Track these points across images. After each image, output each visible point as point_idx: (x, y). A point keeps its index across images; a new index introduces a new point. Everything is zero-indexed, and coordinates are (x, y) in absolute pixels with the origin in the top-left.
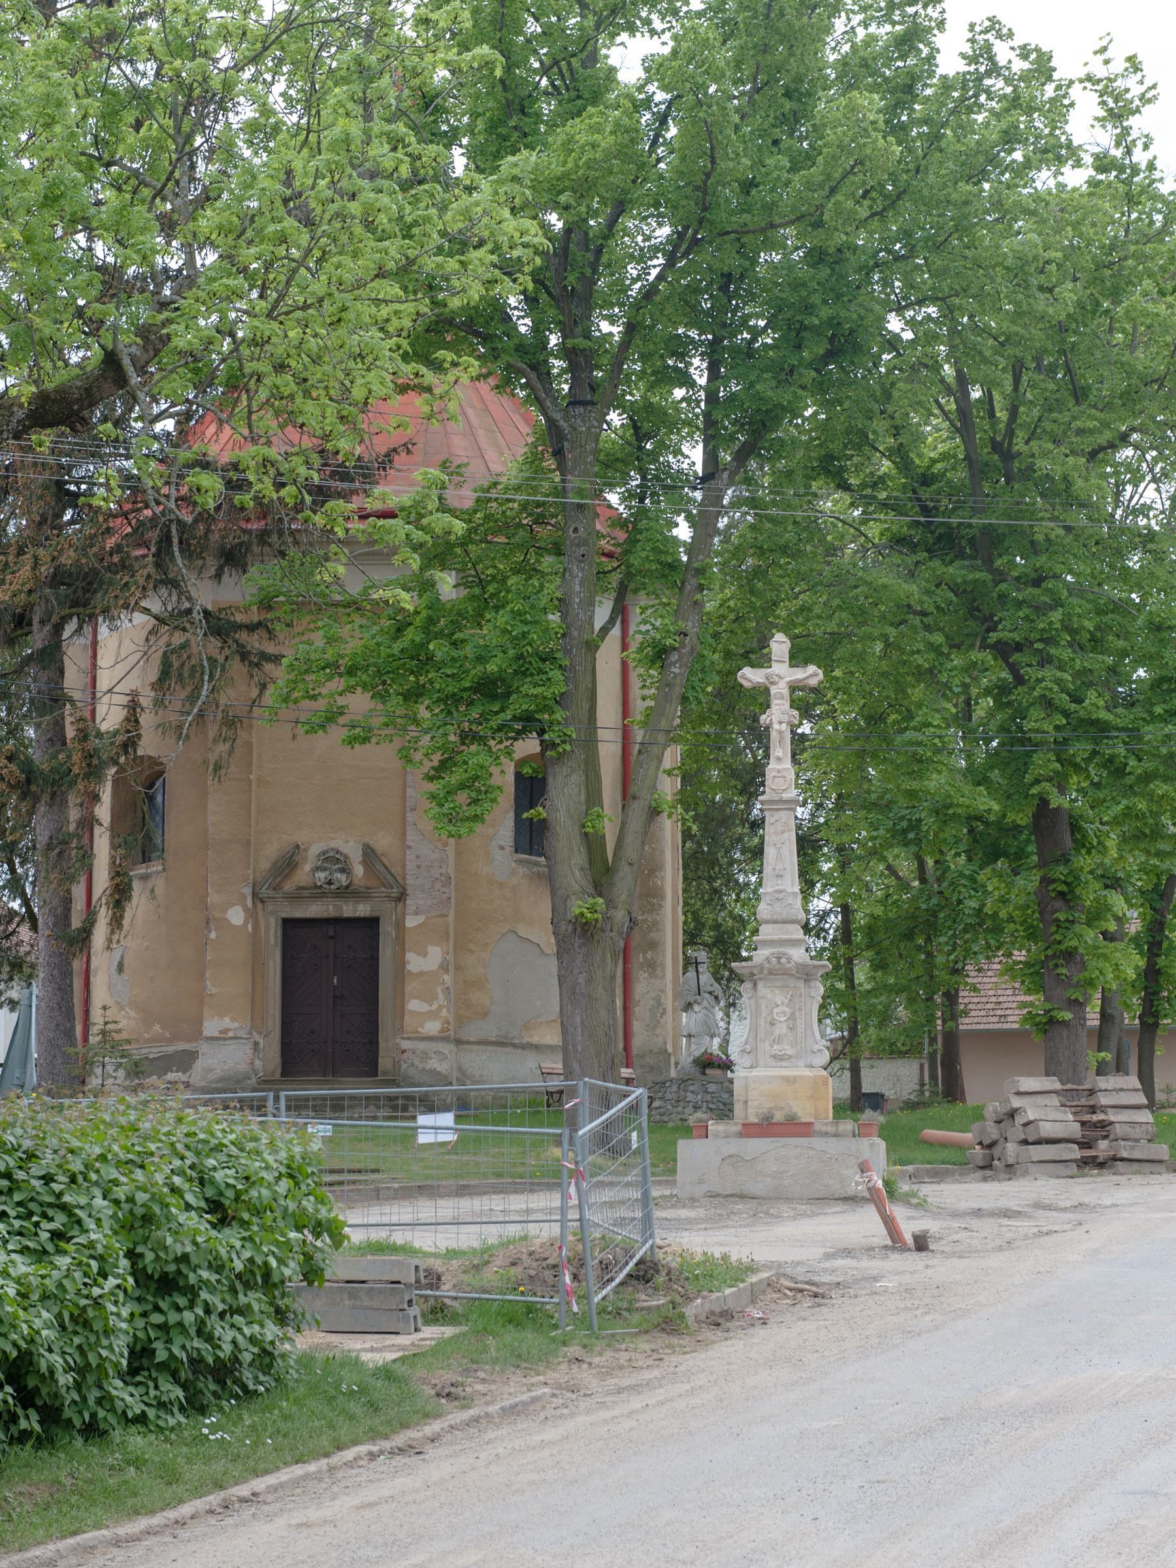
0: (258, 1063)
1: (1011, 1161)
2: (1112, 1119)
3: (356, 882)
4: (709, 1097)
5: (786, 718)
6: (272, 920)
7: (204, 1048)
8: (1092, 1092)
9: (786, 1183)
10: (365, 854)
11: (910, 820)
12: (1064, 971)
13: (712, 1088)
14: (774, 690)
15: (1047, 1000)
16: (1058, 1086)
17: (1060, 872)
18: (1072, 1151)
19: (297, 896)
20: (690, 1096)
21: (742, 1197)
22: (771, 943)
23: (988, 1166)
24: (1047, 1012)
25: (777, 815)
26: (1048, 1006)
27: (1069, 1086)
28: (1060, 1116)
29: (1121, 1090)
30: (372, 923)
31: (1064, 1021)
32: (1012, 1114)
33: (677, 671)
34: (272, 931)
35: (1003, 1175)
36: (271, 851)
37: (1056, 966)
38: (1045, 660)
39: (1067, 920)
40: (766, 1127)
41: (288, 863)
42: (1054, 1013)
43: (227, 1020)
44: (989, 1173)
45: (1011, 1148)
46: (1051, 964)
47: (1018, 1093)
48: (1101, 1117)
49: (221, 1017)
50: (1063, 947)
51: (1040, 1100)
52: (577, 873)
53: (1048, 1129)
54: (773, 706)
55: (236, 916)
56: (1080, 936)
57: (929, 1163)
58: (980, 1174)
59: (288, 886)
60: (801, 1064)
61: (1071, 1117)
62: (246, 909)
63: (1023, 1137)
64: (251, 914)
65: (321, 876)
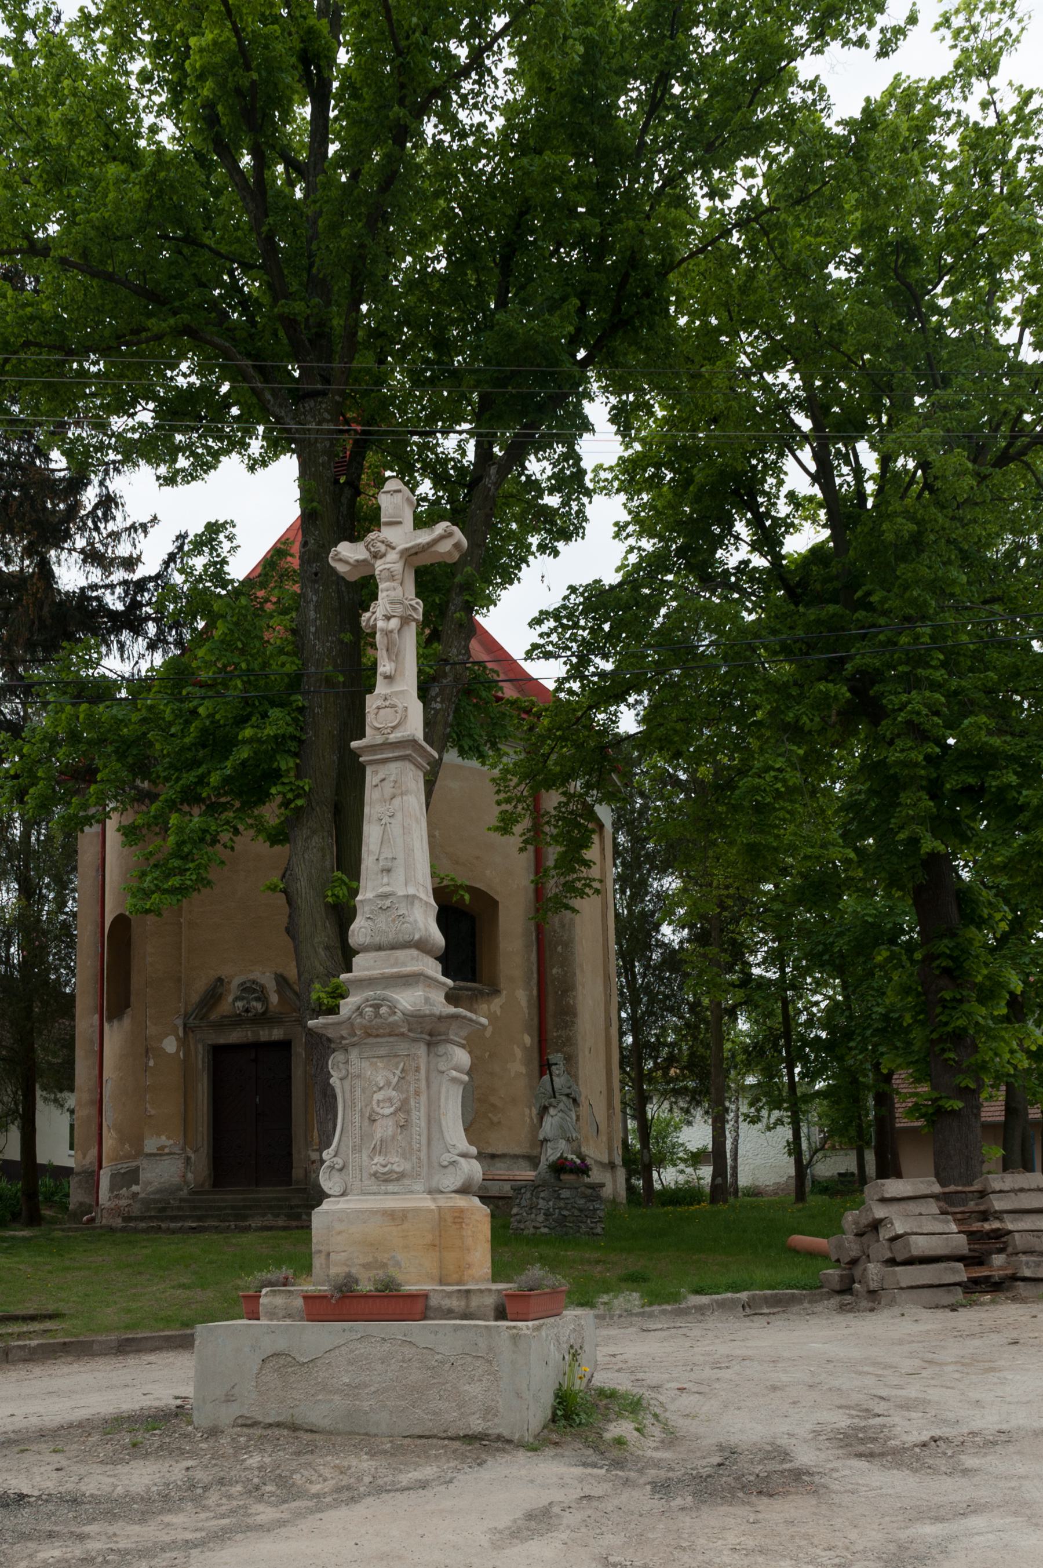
0: (190, 1176)
1: (873, 1286)
2: (1010, 1227)
3: (271, 1008)
4: (562, 1204)
5: (399, 610)
6: (200, 1047)
7: (143, 1163)
8: (983, 1194)
9: (366, 1405)
10: (278, 984)
11: (824, 944)
12: (952, 1055)
13: (565, 1193)
14: (379, 566)
15: (934, 1088)
16: (937, 1189)
17: (944, 945)
18: (954, 1271)
19: (220, 1025)
20: (542, 1204)
21: (294, 1428)
22: (370, 982)
23: (846, 1289)
24: (935, 1101)
25: (383, 771)
26: (935, 1095)
27: (952, 1188)
28: (939, 1227)
29: (1022, 1190)
30: (285, 1046)
31: (953, 1111)
32: (876, 1225)
33: (438, 706)
34: (200, 1057)
35: (864, 1304)
36: (200, 986)
37: (943, 1050)
38: (911, 683)
39: (954, 999)
40: (343, 1303)
41: (214, 995)
42: (940, 1103)
43: (164, 1138)
44: (848, 1298)
45: (874, 1270)
46: (937, 1049)
47: (884, 1200)
48: (996, 1225)
49: (159, 1135)
50: (949, 1029)
51: (913, 1207)
52: (322, 952)
53: (921, 1245)
54: (381, 595)
55: (170, 1045)
56: (969, 1015)
57: (771, 1287)
58: (835, 1301)
59: (214, 1016)
60: (418, 1187)
61: (954, 1228)
62: (178, 1039)
63: (888, 1255)
64: (183, 1043)
65: (239, 1004)
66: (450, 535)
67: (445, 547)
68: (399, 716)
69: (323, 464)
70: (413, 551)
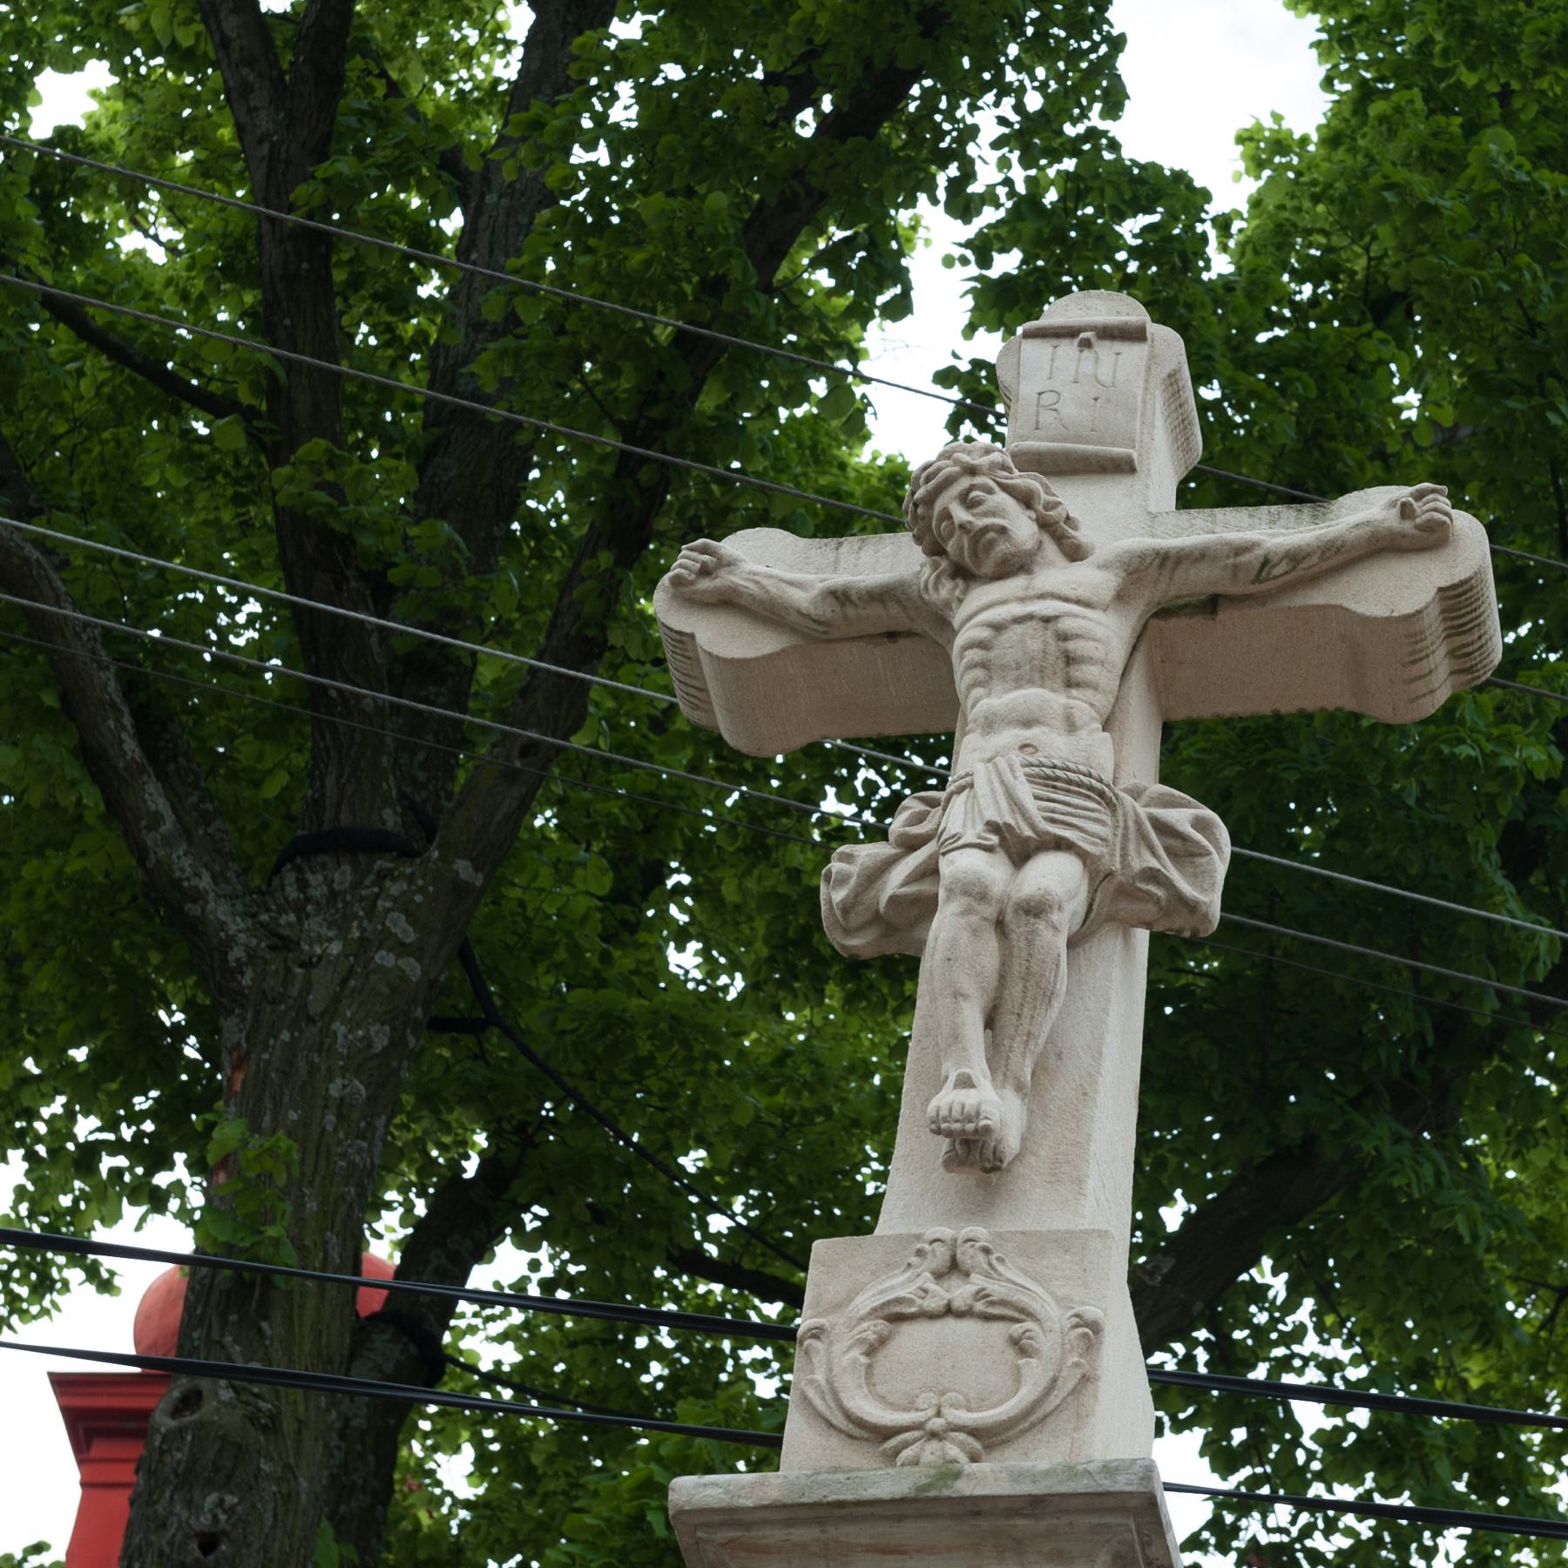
66: (1433, 539)
67: (1400, 591)
68: (1035, 1375)
69: (342, 1108)
70: (1200, 580)
